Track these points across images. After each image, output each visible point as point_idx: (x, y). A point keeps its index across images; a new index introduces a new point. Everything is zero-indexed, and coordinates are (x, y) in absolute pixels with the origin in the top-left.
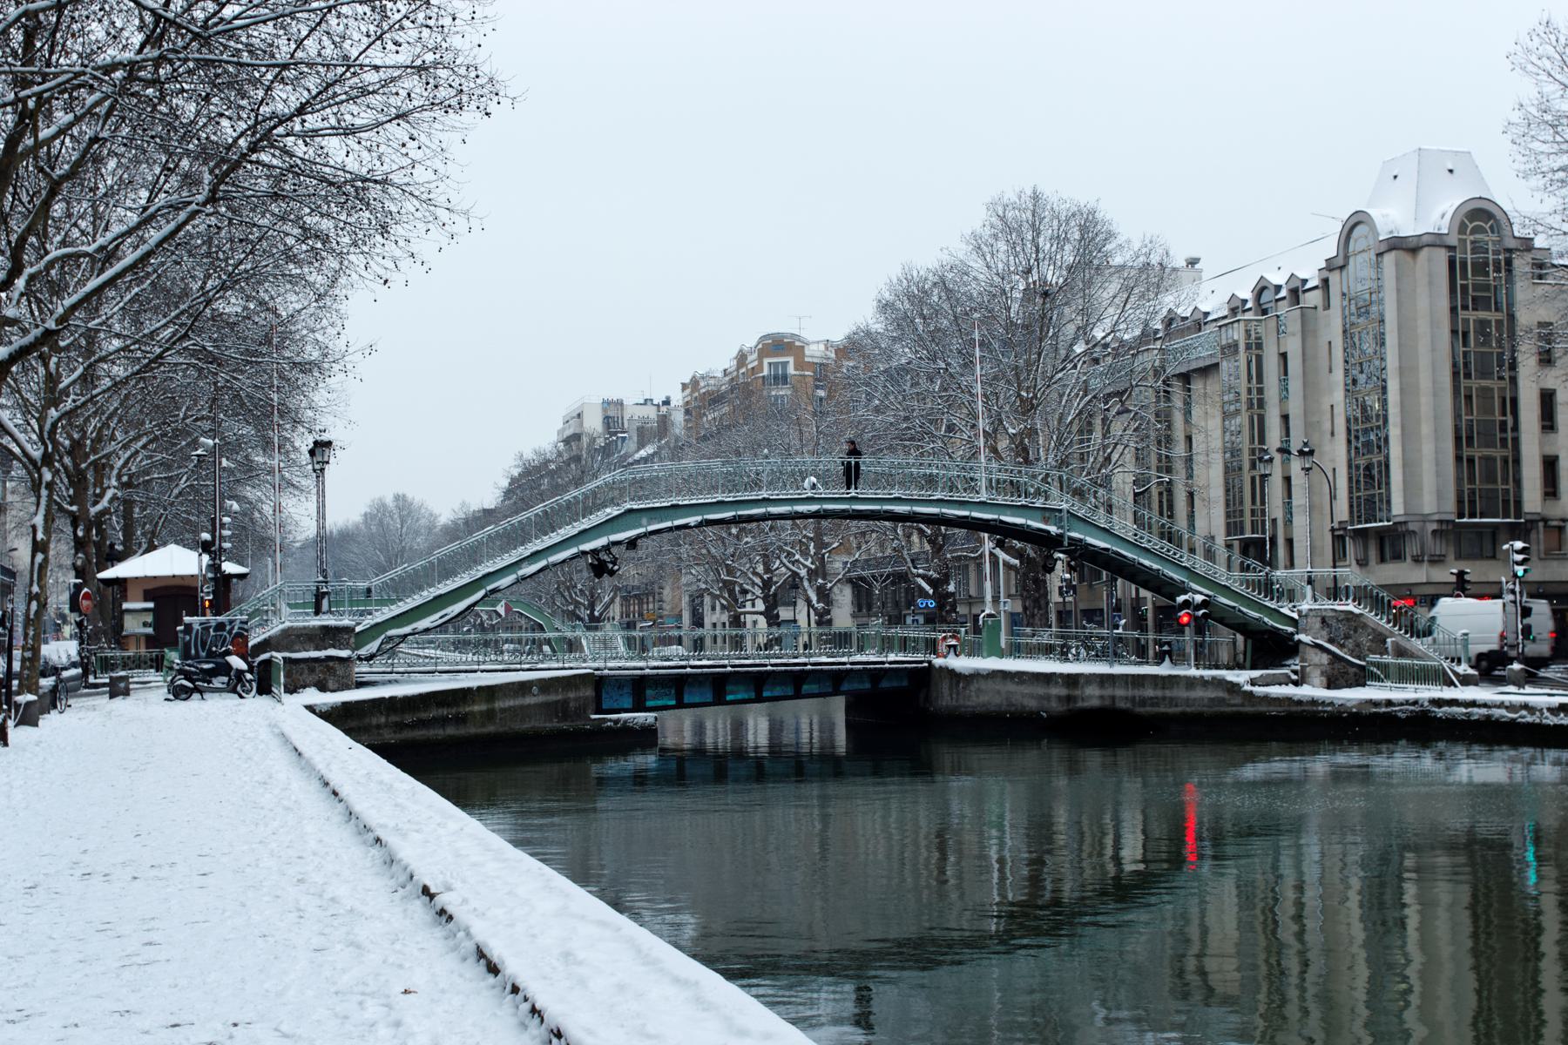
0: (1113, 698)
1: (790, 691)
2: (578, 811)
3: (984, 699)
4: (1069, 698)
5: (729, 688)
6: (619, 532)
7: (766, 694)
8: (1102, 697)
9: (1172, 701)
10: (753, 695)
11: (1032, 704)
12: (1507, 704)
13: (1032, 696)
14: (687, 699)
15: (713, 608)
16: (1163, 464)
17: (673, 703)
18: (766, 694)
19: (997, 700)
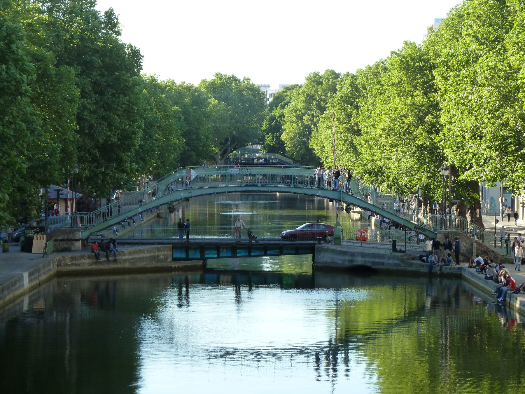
0: (365, 261)
1: (263, 253)
2: (123, 239)
3: (325, 259)
4: (352, 261)
5: (207, 252)
6: (292, 231)
7: (253, 254)
8: (361, 261)
9: (383, 264)
10: (247, 254)
11: (340, 262)
12: (241, 253)
13: (369, 262)
14: (222, 255)
15: (83, 266)
16: (232, 178)
17: (216, 256)
18: (253, 254)
19: (329, 260)
